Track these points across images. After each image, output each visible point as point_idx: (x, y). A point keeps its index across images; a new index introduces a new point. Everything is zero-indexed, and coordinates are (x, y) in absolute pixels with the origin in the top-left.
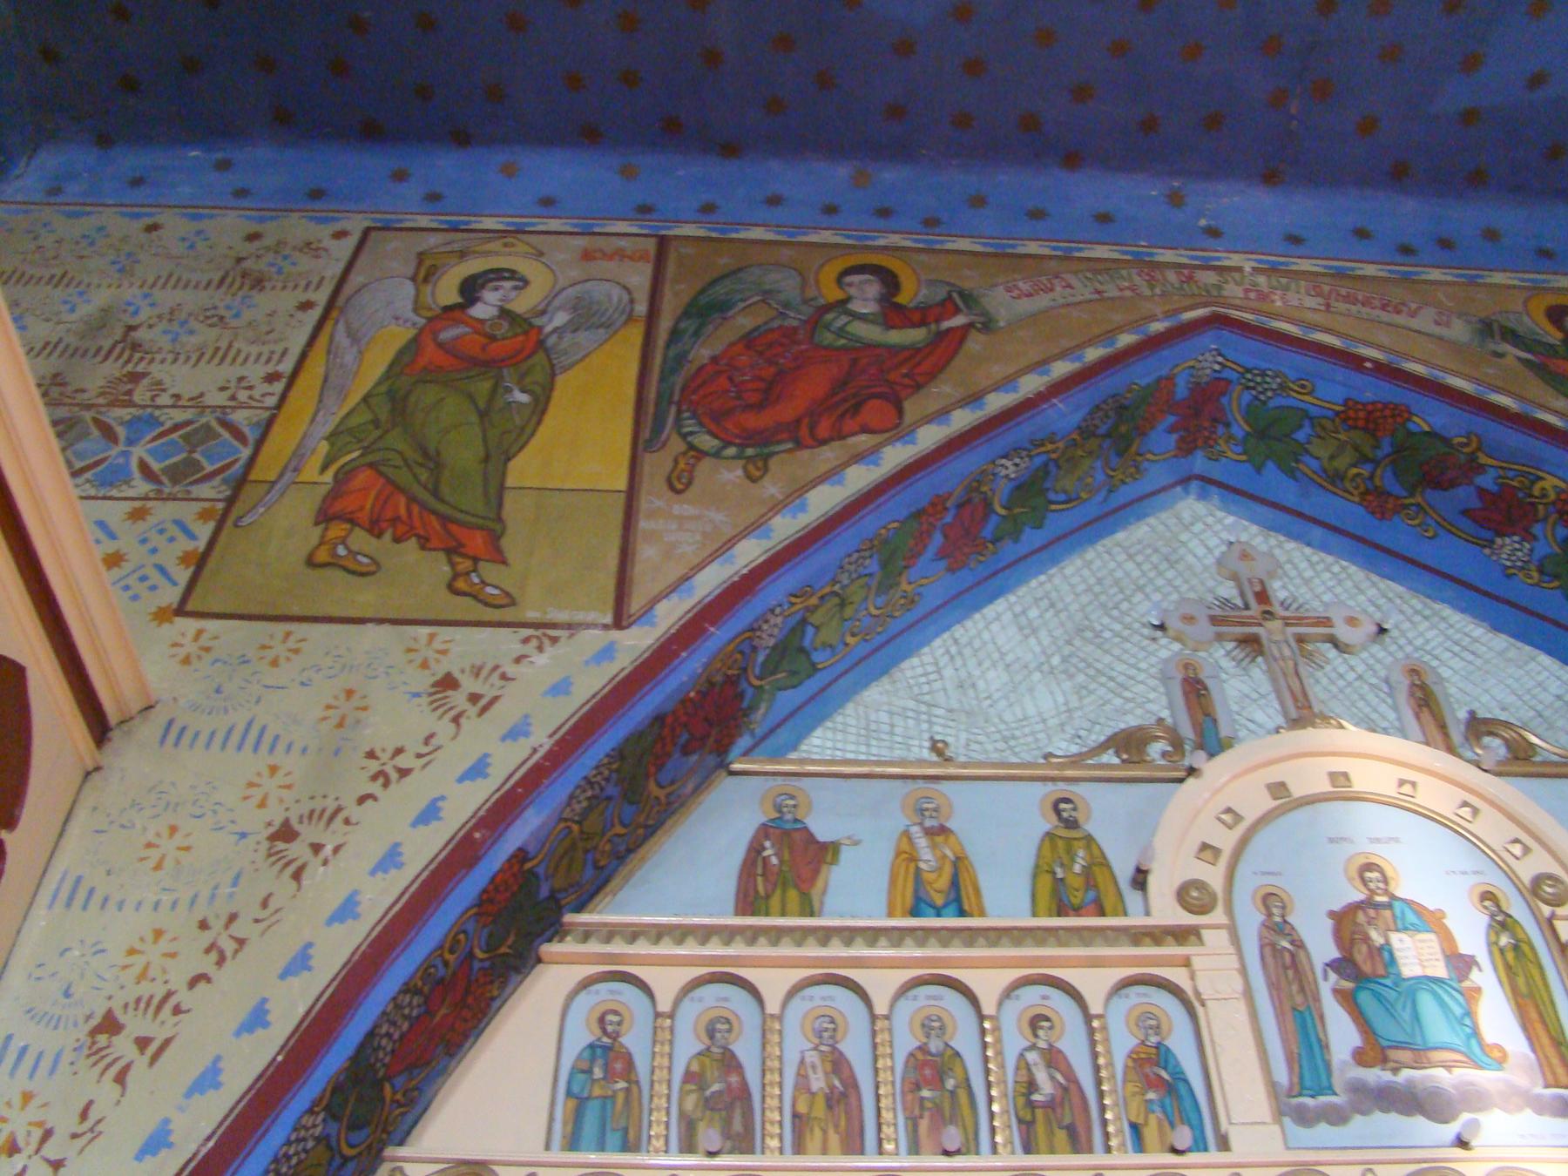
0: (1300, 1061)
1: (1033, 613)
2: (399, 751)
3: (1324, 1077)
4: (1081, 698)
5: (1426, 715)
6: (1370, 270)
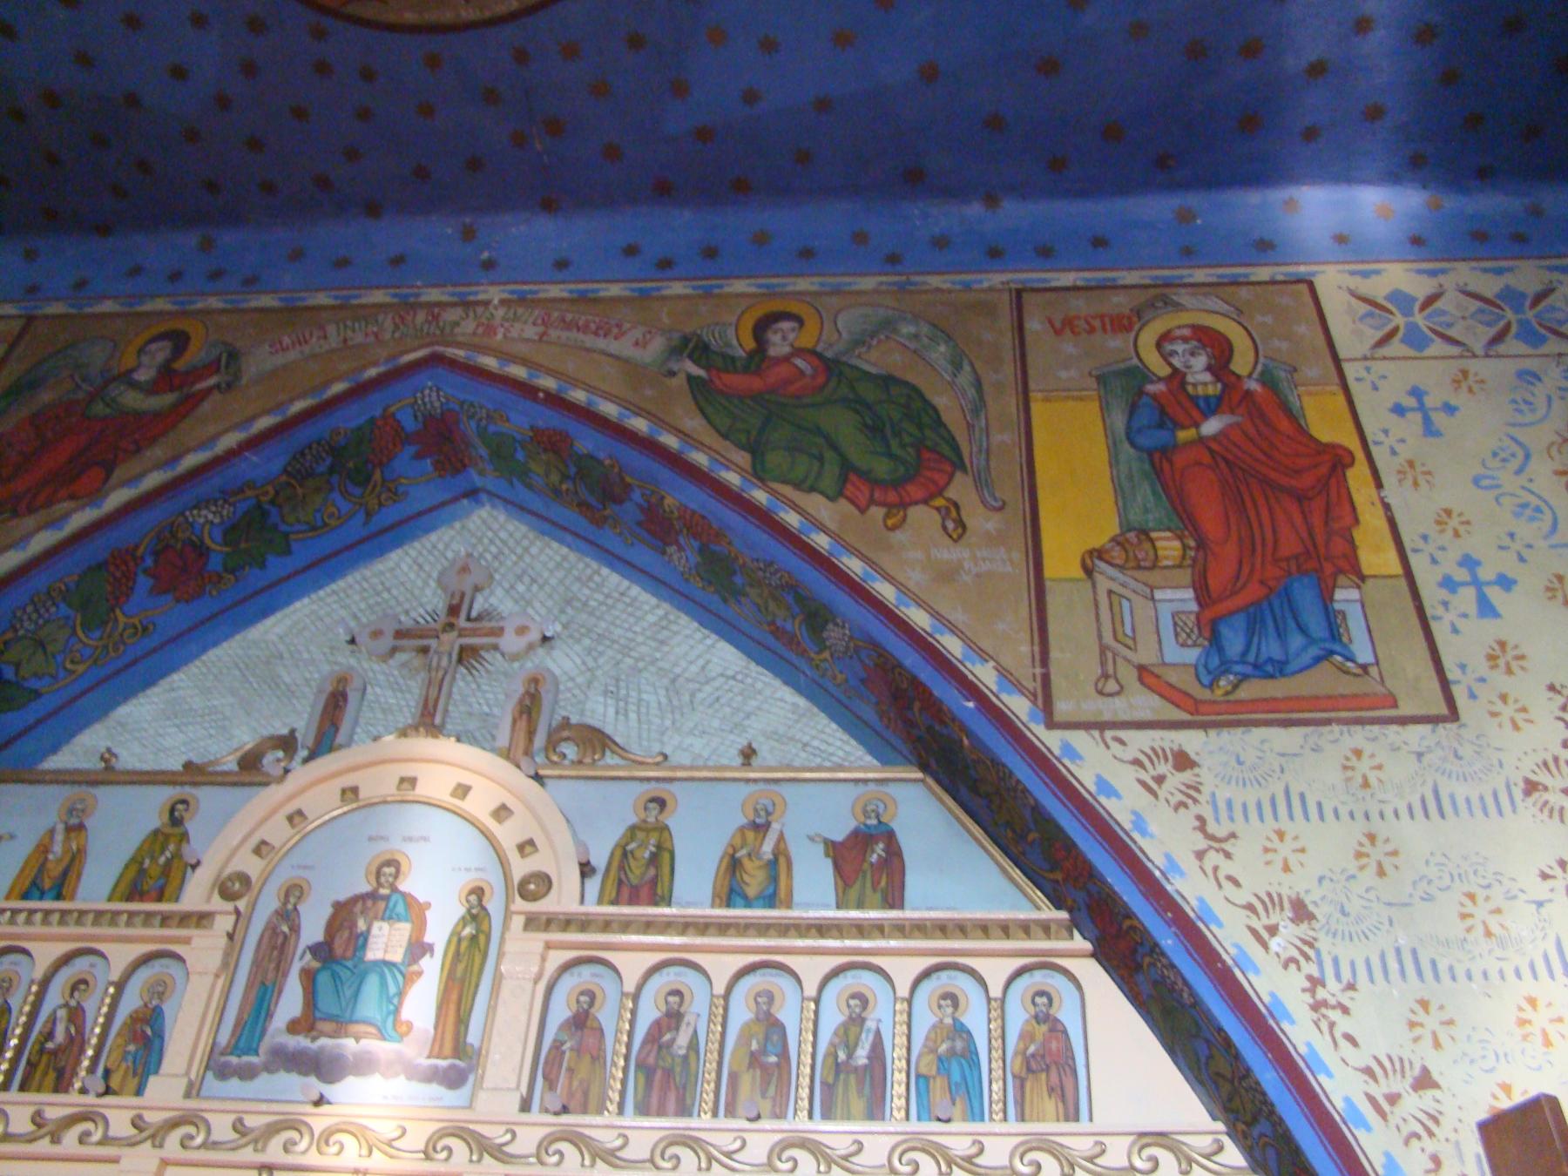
0: (243, 1029)
1: (521, 588)
3: (256, 1039)
4: (595, 660)
5: (523, 724)
6: (615, 290)
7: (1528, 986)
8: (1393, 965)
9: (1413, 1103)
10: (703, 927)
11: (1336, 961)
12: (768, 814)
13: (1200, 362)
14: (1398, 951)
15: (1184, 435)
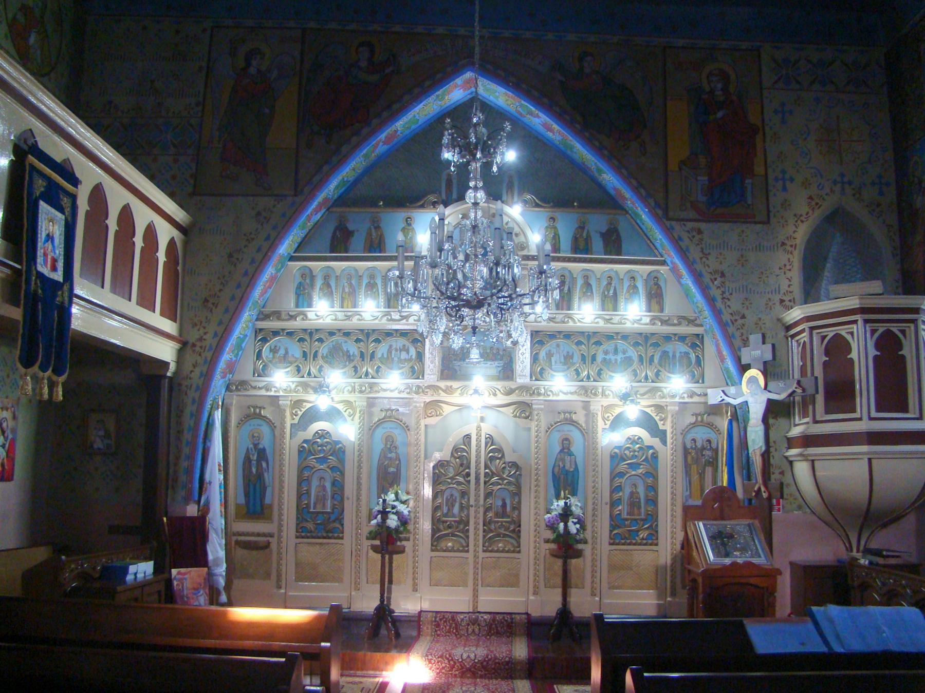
2: (251, 233)
7: (770, 296)
8: (741, 289)
9: (740, 322)
10: (569, 260)
11: (729, 287)
12: (584, 224)
13: (720, 86)
14: (743, 286)
15: (711, 117)
